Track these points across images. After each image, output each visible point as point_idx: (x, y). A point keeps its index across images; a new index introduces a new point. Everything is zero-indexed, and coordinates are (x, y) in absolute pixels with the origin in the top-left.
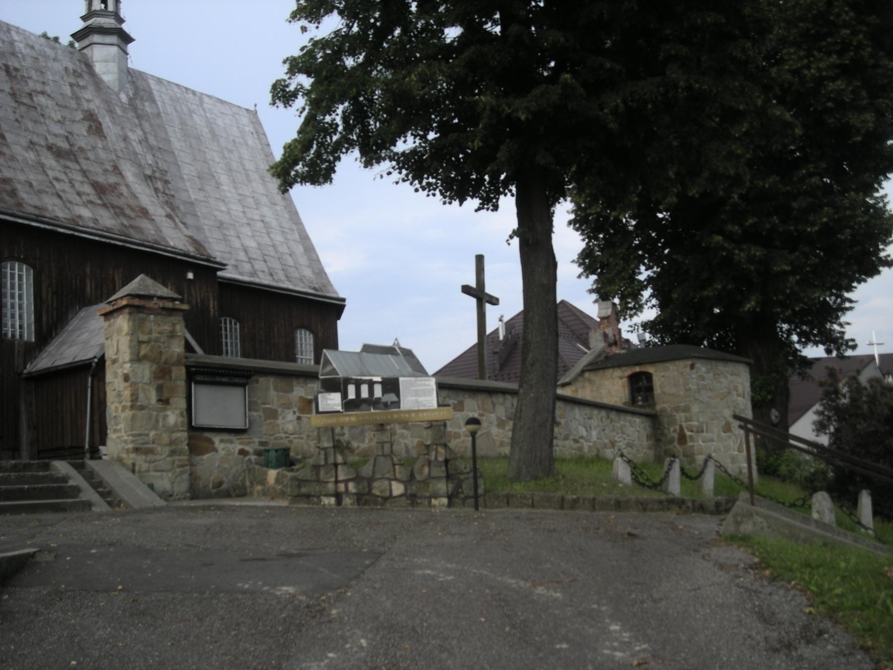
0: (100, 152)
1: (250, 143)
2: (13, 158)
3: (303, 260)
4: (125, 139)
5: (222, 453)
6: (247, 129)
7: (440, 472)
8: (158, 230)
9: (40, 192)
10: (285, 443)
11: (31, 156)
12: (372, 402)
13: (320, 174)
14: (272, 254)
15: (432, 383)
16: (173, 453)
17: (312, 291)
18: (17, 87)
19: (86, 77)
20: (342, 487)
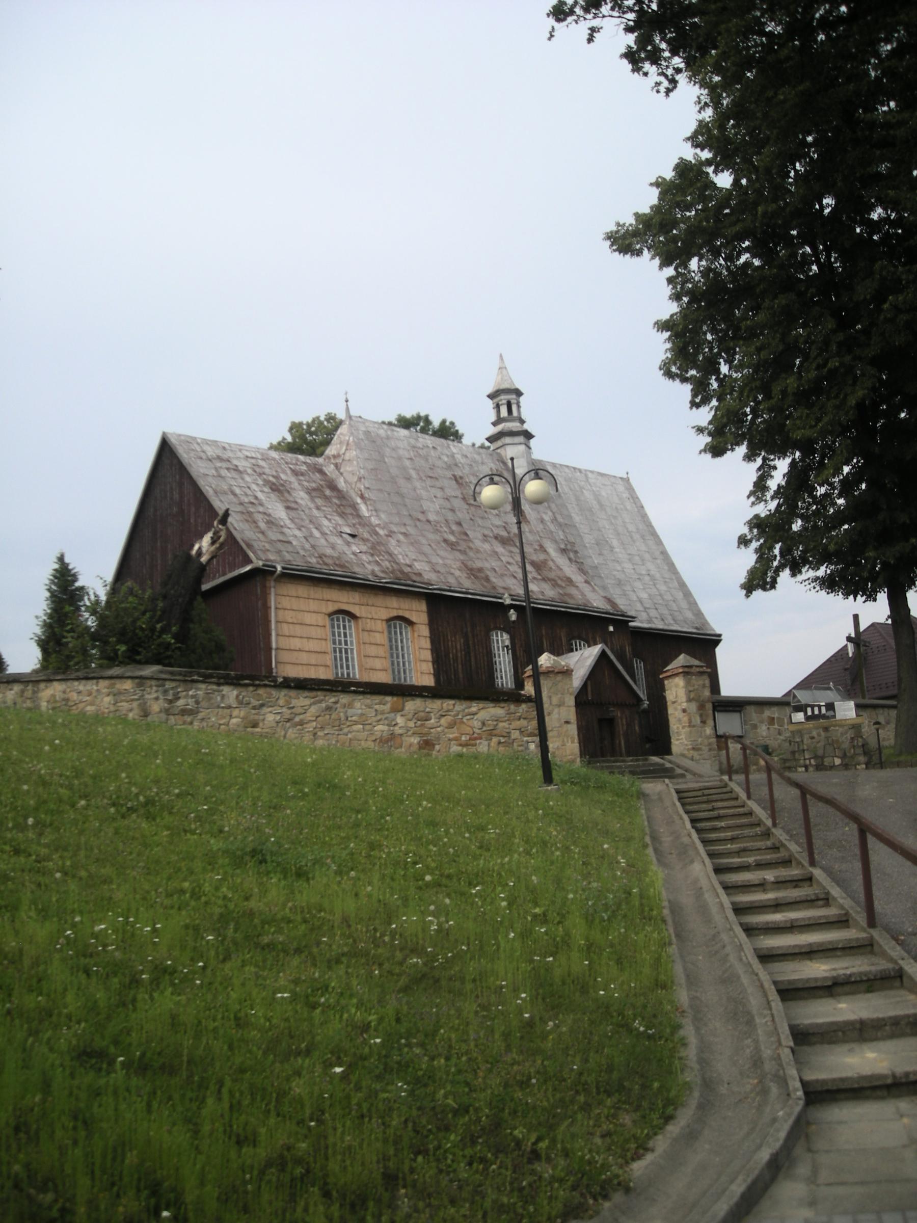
1: (628, 507)
2: (478, 551)
3: (684, 605)
4: (542, 521)
6: (624, 495)
7: (860, 751)
8: (583, 594)
9: (502, 575)
11: (487, 546)
12: (821, 716)
14: (661, 602)
16: (710, 750)
17: (694, 631)
18: (465, 492)
20: (807, 762)
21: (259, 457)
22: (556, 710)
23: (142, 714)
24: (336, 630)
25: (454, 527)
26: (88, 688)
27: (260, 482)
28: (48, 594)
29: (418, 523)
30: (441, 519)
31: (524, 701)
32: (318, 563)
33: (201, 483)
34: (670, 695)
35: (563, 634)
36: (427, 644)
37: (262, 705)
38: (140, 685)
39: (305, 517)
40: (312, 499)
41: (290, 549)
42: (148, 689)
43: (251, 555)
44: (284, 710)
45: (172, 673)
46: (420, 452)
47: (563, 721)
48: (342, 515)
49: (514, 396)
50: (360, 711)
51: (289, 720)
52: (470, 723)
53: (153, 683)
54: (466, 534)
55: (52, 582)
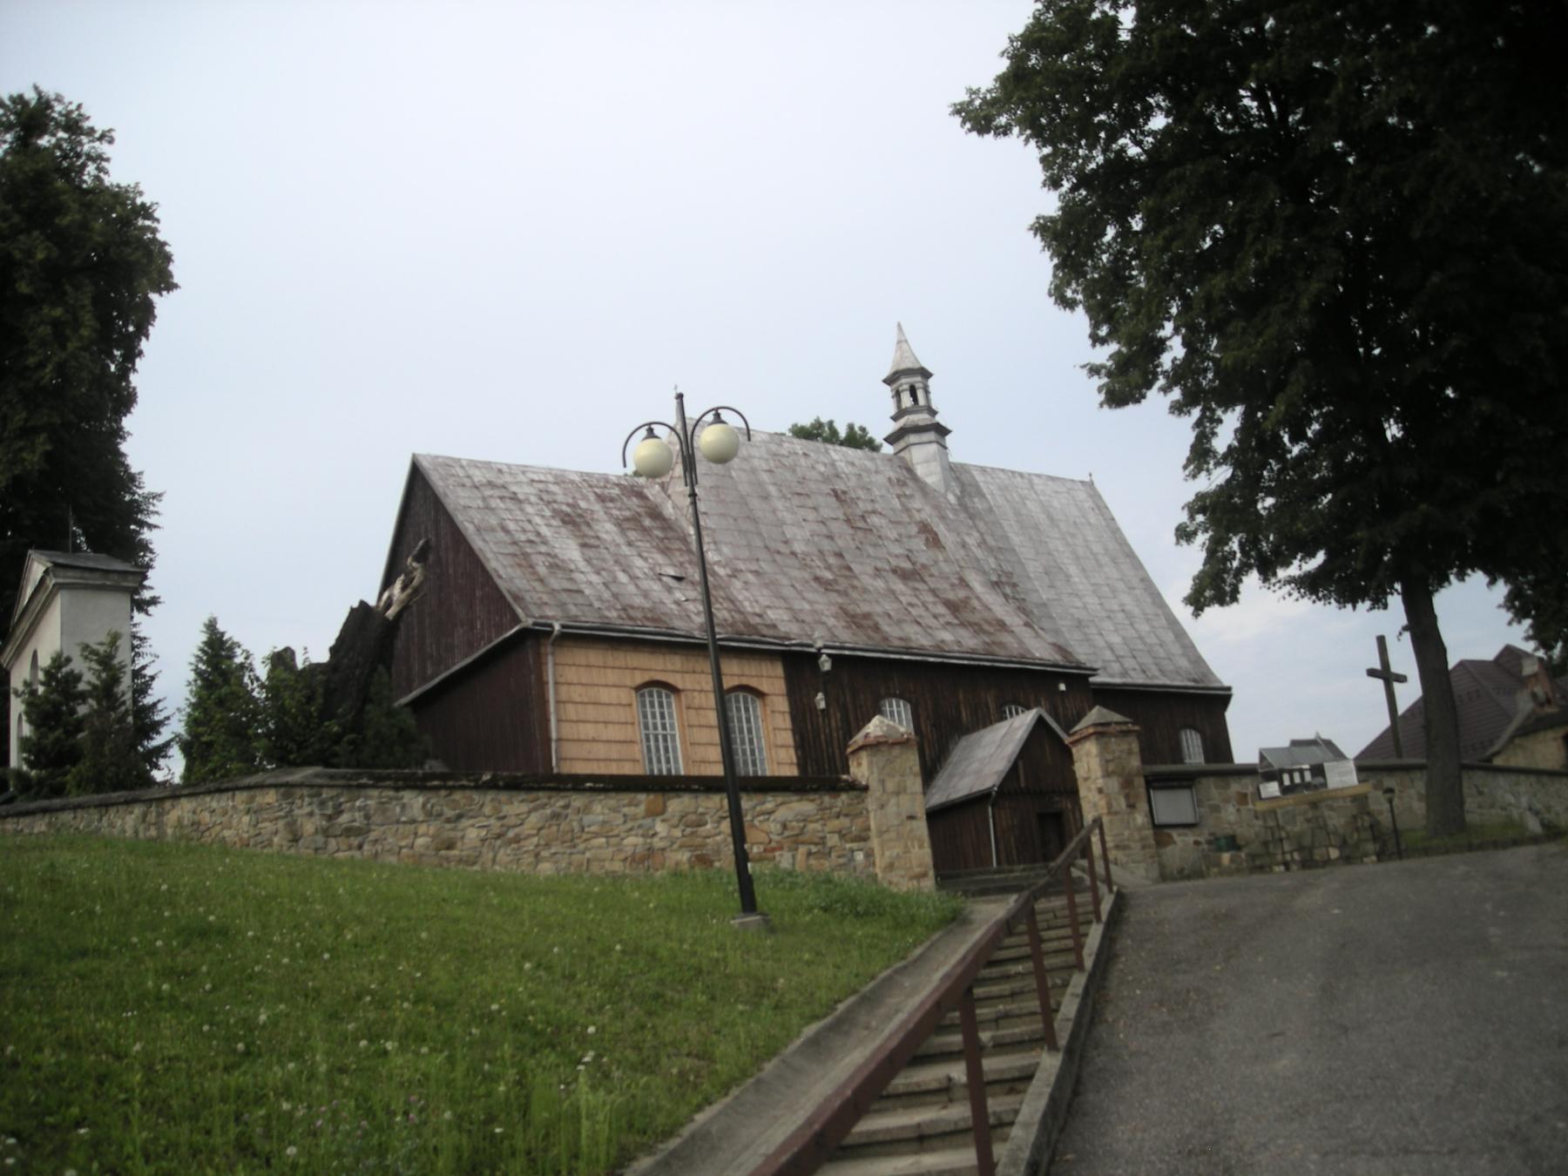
0: (942, 564)
2: (865, 590)
3: (1176, 649)
4: (964, 545)
5: (1180, 844)
7: (1367, 835)
8: (1020, 642)
9: (899, 622)
10: (1229, 832)
11: (880, 584)
12: (1307, 786)
13: (1226, 596)
14: (1140, 647)
15: (1352, 765)
16: (1144, 847)
18: (849, 511)
19: (910, 483)
20: (1288, 857)
21: (550, 479)
22: (893, 801)
23: (290, 837)
24: (648, 709)
25: (832, 560)
26: (223, 804)
27: (548, 513)
28: (192, 676)
29: (778, 557)
30: (813, 550)
31: (843, 790)
32: (620, 617)
33: (460, 518)
34: (1080, 769)
35: (990, 699)
36: (785, 722)
37: (460, 817)
38: (286, 796)
39: (607, 556)
40: (623, 531)
41: (580, 600)
42: (298, 802)
43: (519, 611)
44: (492, 821)
45: (332, 777)
46: (785, 461)
47: (904, 816)
48: (665, 551)
49: (919, 379)
50: (601, 818)
51: (499, 836)
52: (765, 826)
53: (305, 791)
54: (849, 569)
55: (200, 659)
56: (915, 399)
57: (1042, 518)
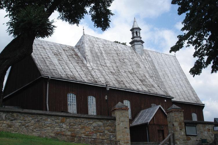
2: (122, 75)
21: (53, 44)
30: (111, 66)
50: (50, 122)
51: (24, 125)
56: (137, 35)
57: (163, 63)
